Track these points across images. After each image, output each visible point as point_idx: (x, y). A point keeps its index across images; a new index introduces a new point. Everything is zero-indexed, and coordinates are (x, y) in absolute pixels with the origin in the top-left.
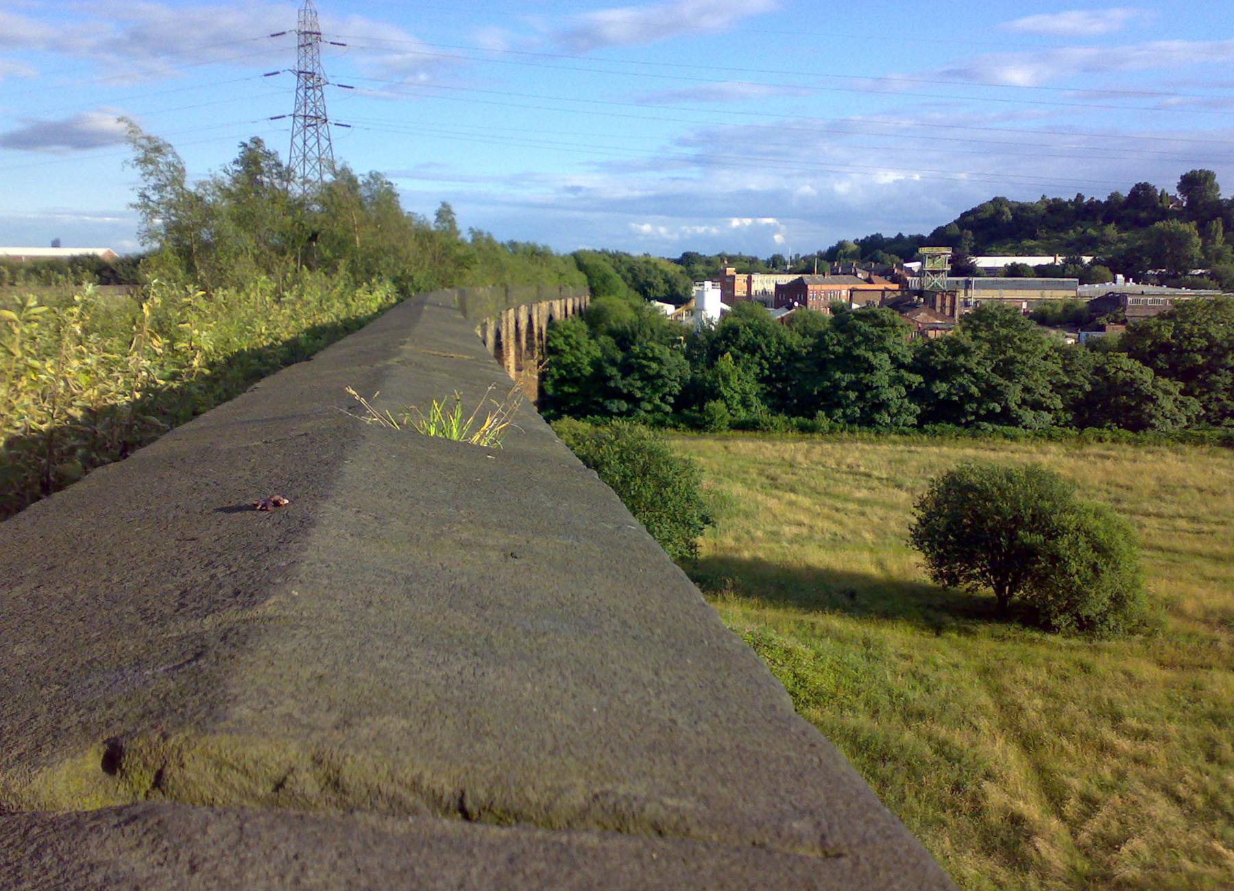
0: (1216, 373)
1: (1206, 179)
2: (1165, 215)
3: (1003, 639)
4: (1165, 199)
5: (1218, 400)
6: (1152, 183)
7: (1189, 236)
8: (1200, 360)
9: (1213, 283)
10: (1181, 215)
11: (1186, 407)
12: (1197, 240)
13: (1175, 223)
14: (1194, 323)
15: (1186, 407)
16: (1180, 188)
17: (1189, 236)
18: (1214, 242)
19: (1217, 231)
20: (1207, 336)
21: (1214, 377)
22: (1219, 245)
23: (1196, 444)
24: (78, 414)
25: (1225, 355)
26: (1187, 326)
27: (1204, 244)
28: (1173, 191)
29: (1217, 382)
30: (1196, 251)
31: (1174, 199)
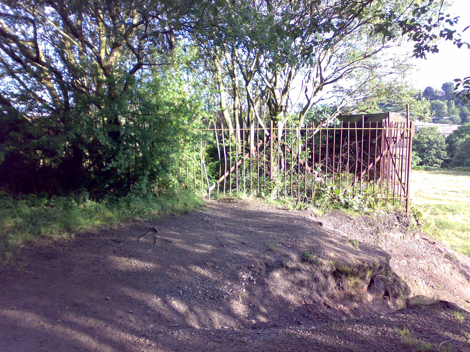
0: (431, 150)
1: (451, 85)
2: (436, 98)
3: (365, 248)
4: (437, 92)
5: (432, 158)
6: (432, 87)
7: (443, 105)
8: (426, 145)
9: (450, 121)
10: (441, 98)
11: (416, 159)
12: (446, 106)
13: (438, 101)
14: (424, 134)
15: (416, 159)
16: (442, 88)
17: (443, 105)
18: (451, 107)
19: (452, 103)
20: (428, 138)
21: (430, 151)
22: (453, 108)
23: (418, 170)
24: (109, 169)
25: (433, 144)
26: (422, 135)
27: (448, 108)
28: (440, 89)
29: (431, 153)
30: (446, 111)
31: (440, 92)
